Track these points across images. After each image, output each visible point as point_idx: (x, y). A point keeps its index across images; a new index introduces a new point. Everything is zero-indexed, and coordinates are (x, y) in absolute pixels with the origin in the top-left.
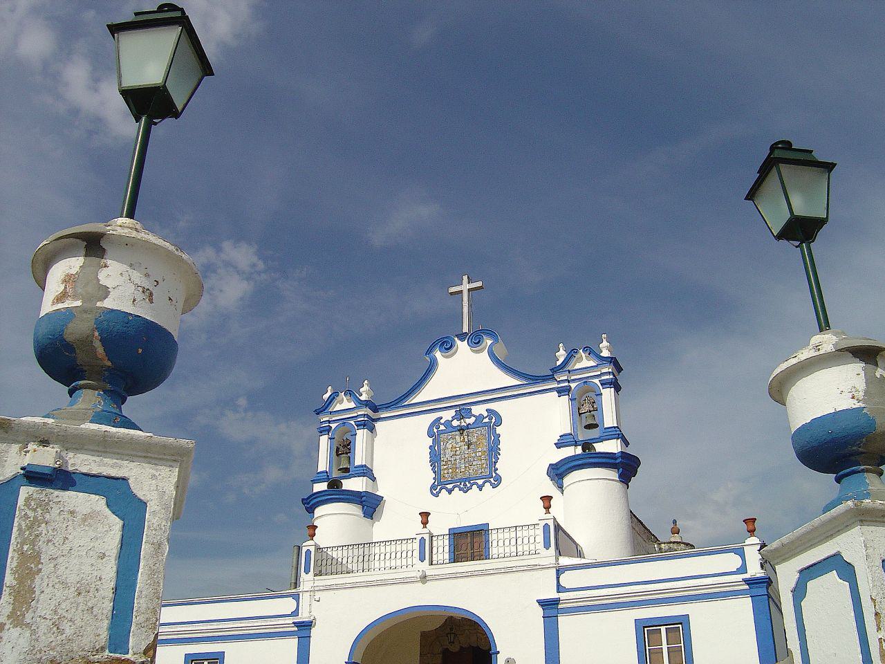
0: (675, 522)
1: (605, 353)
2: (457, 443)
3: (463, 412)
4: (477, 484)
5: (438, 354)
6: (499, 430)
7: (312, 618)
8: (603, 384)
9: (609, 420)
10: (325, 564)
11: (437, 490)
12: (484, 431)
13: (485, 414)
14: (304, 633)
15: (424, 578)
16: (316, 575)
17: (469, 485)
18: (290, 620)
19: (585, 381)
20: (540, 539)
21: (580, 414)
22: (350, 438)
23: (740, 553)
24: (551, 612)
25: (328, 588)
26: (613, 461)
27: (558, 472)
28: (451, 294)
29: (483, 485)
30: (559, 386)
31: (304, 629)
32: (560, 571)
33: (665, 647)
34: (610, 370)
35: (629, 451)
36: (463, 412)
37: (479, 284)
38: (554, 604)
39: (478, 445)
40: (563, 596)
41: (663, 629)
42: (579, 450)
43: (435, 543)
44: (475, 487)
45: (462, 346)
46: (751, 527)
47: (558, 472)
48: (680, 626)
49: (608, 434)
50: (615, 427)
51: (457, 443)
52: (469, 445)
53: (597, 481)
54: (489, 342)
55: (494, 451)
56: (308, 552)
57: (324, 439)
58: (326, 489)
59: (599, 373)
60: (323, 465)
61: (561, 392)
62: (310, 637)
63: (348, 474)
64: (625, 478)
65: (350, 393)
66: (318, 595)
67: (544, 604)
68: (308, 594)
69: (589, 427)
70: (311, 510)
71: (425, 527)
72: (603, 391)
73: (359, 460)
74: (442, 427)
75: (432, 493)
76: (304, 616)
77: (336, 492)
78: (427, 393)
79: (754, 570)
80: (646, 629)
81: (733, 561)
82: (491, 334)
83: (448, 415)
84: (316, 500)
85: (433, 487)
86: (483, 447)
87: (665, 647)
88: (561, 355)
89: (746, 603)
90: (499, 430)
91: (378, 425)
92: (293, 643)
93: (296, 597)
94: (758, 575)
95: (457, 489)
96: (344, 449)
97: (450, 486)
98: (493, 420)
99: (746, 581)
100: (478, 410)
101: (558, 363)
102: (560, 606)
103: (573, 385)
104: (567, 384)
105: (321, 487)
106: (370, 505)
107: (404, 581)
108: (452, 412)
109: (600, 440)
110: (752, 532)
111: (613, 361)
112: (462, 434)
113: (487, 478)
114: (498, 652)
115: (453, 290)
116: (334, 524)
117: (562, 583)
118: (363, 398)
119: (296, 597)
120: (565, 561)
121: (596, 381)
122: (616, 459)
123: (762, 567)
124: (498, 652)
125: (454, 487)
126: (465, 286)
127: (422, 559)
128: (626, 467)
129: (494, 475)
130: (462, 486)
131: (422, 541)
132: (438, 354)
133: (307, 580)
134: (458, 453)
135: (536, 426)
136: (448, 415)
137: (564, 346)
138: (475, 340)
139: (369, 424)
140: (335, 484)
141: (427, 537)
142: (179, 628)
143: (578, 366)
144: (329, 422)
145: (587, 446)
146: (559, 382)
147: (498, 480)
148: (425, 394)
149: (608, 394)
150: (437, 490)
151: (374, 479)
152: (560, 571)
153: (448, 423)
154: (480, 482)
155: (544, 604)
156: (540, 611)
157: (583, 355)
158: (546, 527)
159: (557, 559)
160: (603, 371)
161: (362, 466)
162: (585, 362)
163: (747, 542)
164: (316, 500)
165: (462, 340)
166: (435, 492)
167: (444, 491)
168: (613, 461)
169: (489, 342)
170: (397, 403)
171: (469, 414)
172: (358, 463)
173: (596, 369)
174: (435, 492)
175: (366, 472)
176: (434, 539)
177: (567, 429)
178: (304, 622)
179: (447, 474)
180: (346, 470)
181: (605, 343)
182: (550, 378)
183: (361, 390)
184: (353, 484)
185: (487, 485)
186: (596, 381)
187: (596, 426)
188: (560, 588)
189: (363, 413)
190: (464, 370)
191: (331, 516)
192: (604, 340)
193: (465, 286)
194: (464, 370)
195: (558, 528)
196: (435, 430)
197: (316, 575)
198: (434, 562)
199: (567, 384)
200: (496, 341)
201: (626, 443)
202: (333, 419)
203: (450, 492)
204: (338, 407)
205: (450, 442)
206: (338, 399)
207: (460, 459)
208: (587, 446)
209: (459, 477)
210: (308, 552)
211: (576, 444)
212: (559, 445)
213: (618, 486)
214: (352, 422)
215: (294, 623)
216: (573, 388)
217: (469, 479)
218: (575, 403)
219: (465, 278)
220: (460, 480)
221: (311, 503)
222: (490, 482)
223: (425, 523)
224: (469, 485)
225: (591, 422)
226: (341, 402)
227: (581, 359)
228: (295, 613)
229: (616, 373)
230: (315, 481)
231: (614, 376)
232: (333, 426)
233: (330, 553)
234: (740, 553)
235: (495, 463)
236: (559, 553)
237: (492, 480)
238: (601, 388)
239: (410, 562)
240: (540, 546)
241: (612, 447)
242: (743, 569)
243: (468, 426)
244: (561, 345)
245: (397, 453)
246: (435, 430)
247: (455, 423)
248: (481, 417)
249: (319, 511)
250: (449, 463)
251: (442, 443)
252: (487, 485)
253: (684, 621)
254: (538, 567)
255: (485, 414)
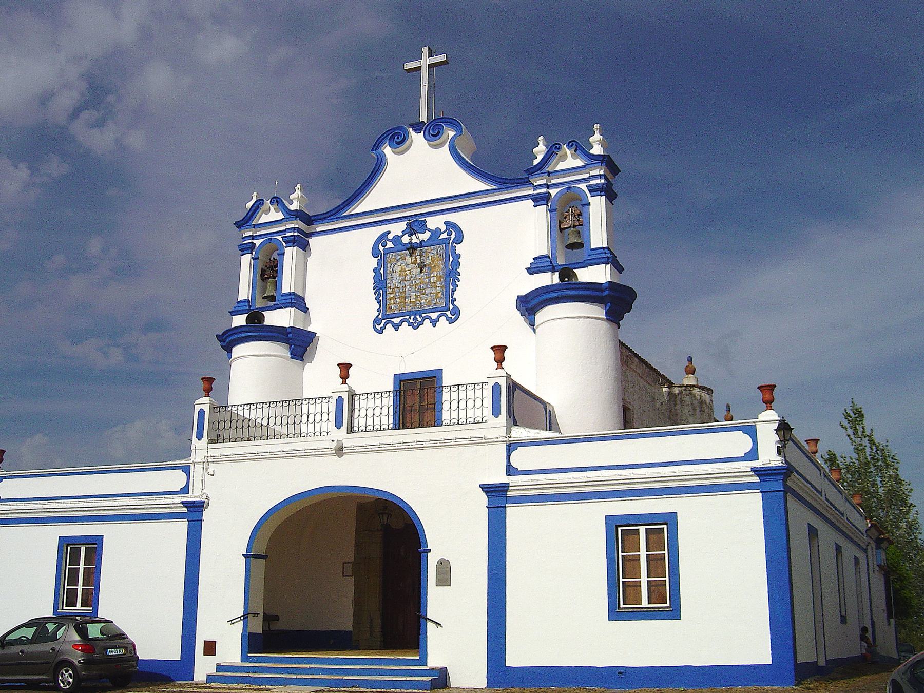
0: (690, 359)
1: (597, 150)
2: (407, 265)
3: (415, 225)
4: (429, 318)
5: (387, 151)
6: (459, 249)
7: (204, 497)
8: (593, 190)
9: (598, 238)
10: (227, 427)
11: (382, 325)
12: (441, 249)
13: (443, 228)
14: (194, 516)
15: (340, 451)
16: (211, 442)
17: (420, 320)
18: (178, 499)
19: (569, 187)
20: (488, 402)
21: (561, 230)
22: (277, 257)
23: (751, 431)
24: (499, 501)
25: (222, 460)
26: (598, 294)
27: (530, 305)
28: (409, 71)
29: (437, 320)
30: (536, 192)
31: (195, 511)
32: (511, 448)
33: (643, 553)
34: (602, 172)
35: (623, 280)
36: (415, 225)
37: (442, 58)
38: (502, 491)
39: (432, 269)
40: (514, 480)
41: (642, 530)
42: (556, 279)
43: (357, 403)
44: (427, 322)
45: (417, 139)
46: (768, 397)
47: (530, 305)
48: (665, 527)
49: (594, 257)
50: (604, 248)
51: (407, 265)
52: (422, 267)
53: (576, 320)
54: (451, 134)
55: (452, 275)
56: (202, 412)
57: (246, 259)
58: (245, 324)
59: (587, 176)
60: (244, 293)
61: (539, 200)
62: (201, 520)
63: (272, 304)
64: (615, 316)
65: (276, 201)
66: (212, 468)
67: (488, 489)
68: (201, 466)
69: (571, 246)
70: (228, 349)
71: (344, 382)
72: (591, 200)
73: (287, 285)
74: (390, 245)
75: (375, 329)
76: (194, 495)
77: (256, 329)
78: (377, 198)
79: (769, 457)
80: (620, 529)
81: (739, 443)
82: (453, 124)
83: (397, 229)
84: (236, 336)
85: (376, 321)
86: (437, 273)
87: (643, 553)
88: (540, 150)
89: (753, 502)
90: (459, 249)
91: (313, 241)
92: (182, 526)
93: (186, 470)
94: (773, 464)
95: (405, 324)
96: (269, 271)
97: (396, 321)
98: (453, 236)
99: (757, 471)
100: (435, 223)
101: (536, 162)
102: (509, 494)
103: (553, 192)
104: (544, 190)
105: (240, 320)
106: (300, 343)
107: (317, 453)
108: (403, 226)
109: (584, 265)
110: (769, 403)
111: (605, 160)
112: (411, 254)
113: (443, 311)
114: (430, 550)
115: (409, 66)
116: (252, 372)
117: (514, 463)
118: (293, 207)
119: (186, 470)
120: (519, 433)
121: (583, 186)
122: (602, 291)
123: (779, 453)
124: (430, 550)
125: (402, 321)
126: (425, 61)
127: (338, 425)
128: (616, 301)
129: (451, 307)
130: (411, 321)
131: (340, 401)
132: (387, 151)
133: (200, 448)
134: (408, 278)
135: (506, 240)
136: (397, 229)
137: (546, 139)
138: (433, 131)
139: (301, 242)
140: (255, 318)
141: (345, 396)
142: (54, 504)
143: (561, 166)
144: (253, 237)
145: (566, 273)
146: (536, 187)
147: (457, 312)
148: (368, 203)
149: (597, 206)
150: (382, 325)
151: (306, 310)
152: (511, 448)
153: (397, 239)
154: (434, 316)
155: (488, 489)
156: (483, 499)
157: (568, 152)
158: (496, 388)
159: (509, 431)
160: (593, 173)
161: (290, 294)
162: (570, 161)
163: (762, 417)
164: (236, 336)
165: (417, 131)
166: (378, 327)
167: (389, 325)
168: (598, 294)
169: (451, 134)
170: (334, 214)
171: (423, 227)
172: (285, 289)
173: (583, 170)
174: (378, 327)
175: (297, 302)
176: (357, 398)
177: (544, 251)
178: (194, 502)
179: (394, 305)
180: (272, 298)
181: (597, 136)
182: (525, 182)
183: (292, 197)
184: (279, 318)
185: (443, 319)
186: (583, 186)
187: (580, 245)
188: (510, 470)
189: (292, 226)
190: (421, 171)
191: (251, 358)
192: (597, 132)
193: (425, 61)
194: (421, 171)
195: (513, 387)
196: (381, 248)
197: (211, 442)
198: (356, 429)
199: (544, 190)
200: (459, 132)
201: (618, 268)
202: (258, 233)
203: (397, 327)
204: (264, 219)
205: (399, 264)
206: (264, 208)
207: (411, 286)
208: (566, 273)
209: (409, 309)
210: (202, 412)
211: (553, 270)
212: (531, 271)
213: (605, 326)
214: (279, 238)
215: (182, 503)
216: (553, 196)
217: (420, 313)
218: (555, 214)
219: (425, 50)
220: (410, 313)
221: (229, 340)
222: (446, 316)
223: (345, 377)
224: (420, 320)
225: (574, 240)
226: (267, 212)
227: (564, 157)
228: (185, 490)
229: (609, 176)
230: (233, 313)
231: (606, 178)
232: (258, 242)
233: (240, 413)
234: (751, 431)
235: (453, 291)
236: (514, 420)
237: (448, 313)
238: (589, 195)
239: (324, 429)
240: (488, 412)
241: (598, 274)
242: (753, 454)
243: (422, 244)
244: (541, 138)
245: (335, 275)
246: (381, 248)
247: (406, 239)
248: (437, 232)
249: (238, 350)
250: (397, 290)
251: (389, 265)
252: (443, 319)
253: (671, 519)
254: (484, 441)
255: (443, 228)
